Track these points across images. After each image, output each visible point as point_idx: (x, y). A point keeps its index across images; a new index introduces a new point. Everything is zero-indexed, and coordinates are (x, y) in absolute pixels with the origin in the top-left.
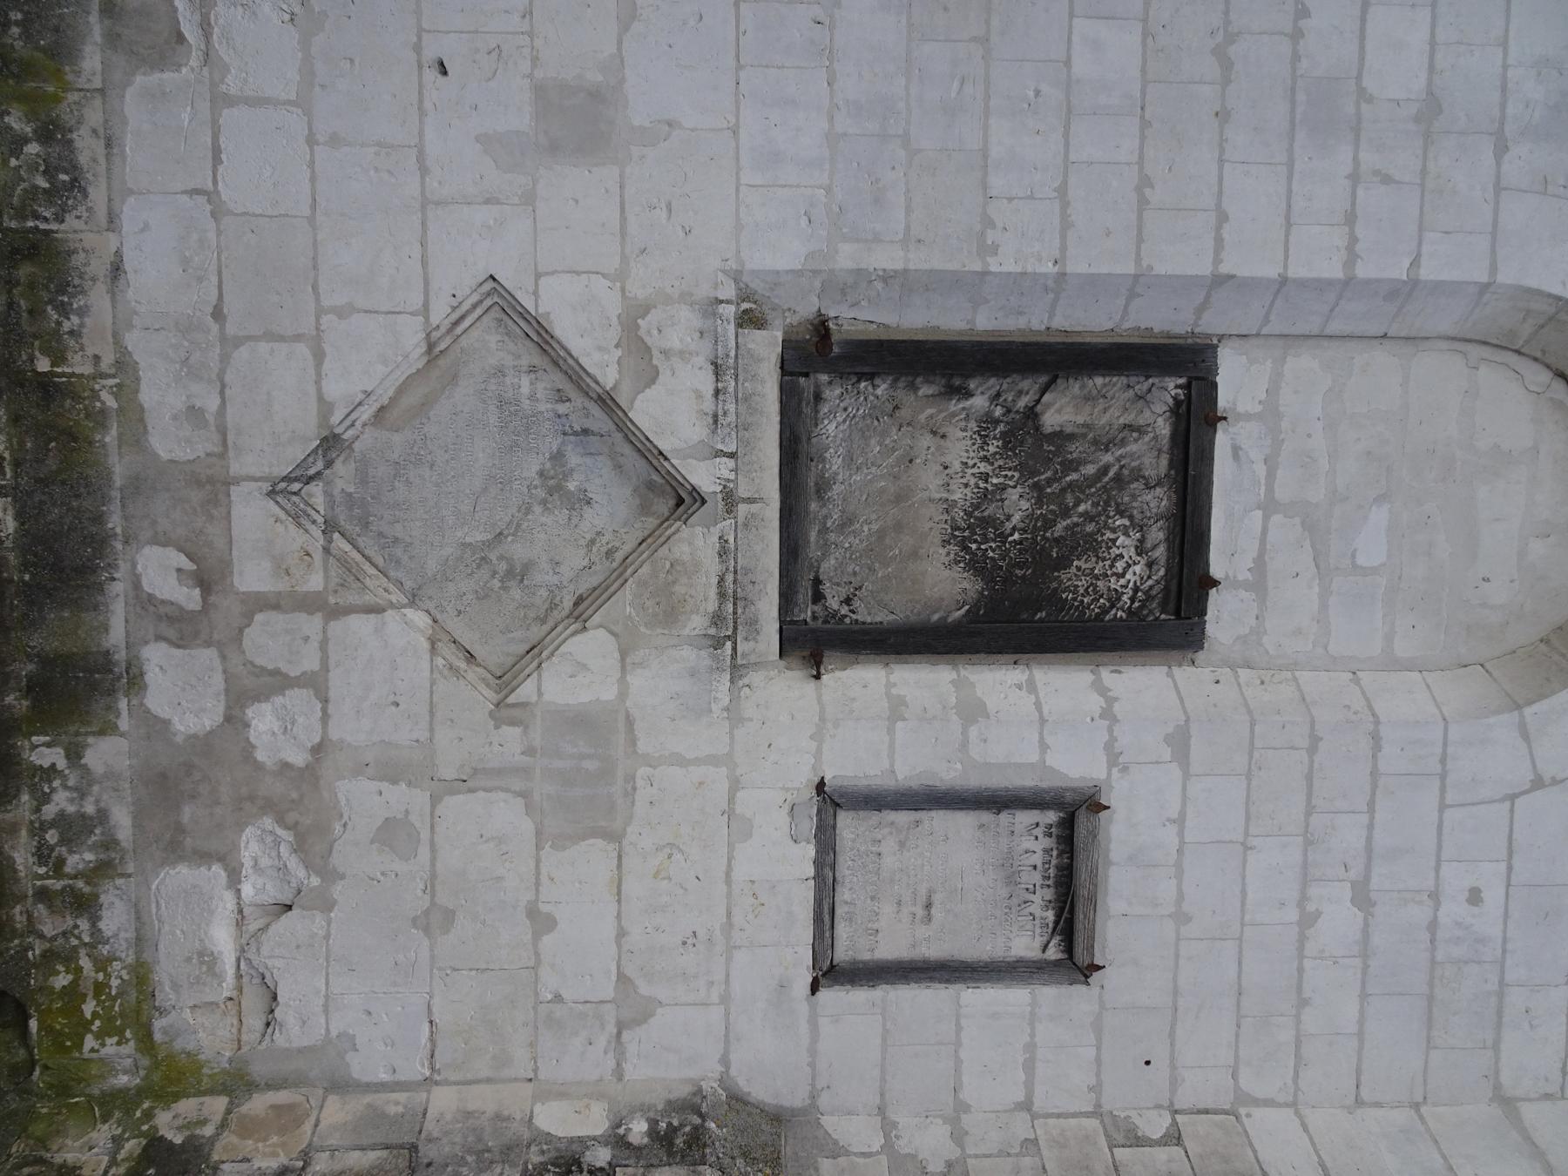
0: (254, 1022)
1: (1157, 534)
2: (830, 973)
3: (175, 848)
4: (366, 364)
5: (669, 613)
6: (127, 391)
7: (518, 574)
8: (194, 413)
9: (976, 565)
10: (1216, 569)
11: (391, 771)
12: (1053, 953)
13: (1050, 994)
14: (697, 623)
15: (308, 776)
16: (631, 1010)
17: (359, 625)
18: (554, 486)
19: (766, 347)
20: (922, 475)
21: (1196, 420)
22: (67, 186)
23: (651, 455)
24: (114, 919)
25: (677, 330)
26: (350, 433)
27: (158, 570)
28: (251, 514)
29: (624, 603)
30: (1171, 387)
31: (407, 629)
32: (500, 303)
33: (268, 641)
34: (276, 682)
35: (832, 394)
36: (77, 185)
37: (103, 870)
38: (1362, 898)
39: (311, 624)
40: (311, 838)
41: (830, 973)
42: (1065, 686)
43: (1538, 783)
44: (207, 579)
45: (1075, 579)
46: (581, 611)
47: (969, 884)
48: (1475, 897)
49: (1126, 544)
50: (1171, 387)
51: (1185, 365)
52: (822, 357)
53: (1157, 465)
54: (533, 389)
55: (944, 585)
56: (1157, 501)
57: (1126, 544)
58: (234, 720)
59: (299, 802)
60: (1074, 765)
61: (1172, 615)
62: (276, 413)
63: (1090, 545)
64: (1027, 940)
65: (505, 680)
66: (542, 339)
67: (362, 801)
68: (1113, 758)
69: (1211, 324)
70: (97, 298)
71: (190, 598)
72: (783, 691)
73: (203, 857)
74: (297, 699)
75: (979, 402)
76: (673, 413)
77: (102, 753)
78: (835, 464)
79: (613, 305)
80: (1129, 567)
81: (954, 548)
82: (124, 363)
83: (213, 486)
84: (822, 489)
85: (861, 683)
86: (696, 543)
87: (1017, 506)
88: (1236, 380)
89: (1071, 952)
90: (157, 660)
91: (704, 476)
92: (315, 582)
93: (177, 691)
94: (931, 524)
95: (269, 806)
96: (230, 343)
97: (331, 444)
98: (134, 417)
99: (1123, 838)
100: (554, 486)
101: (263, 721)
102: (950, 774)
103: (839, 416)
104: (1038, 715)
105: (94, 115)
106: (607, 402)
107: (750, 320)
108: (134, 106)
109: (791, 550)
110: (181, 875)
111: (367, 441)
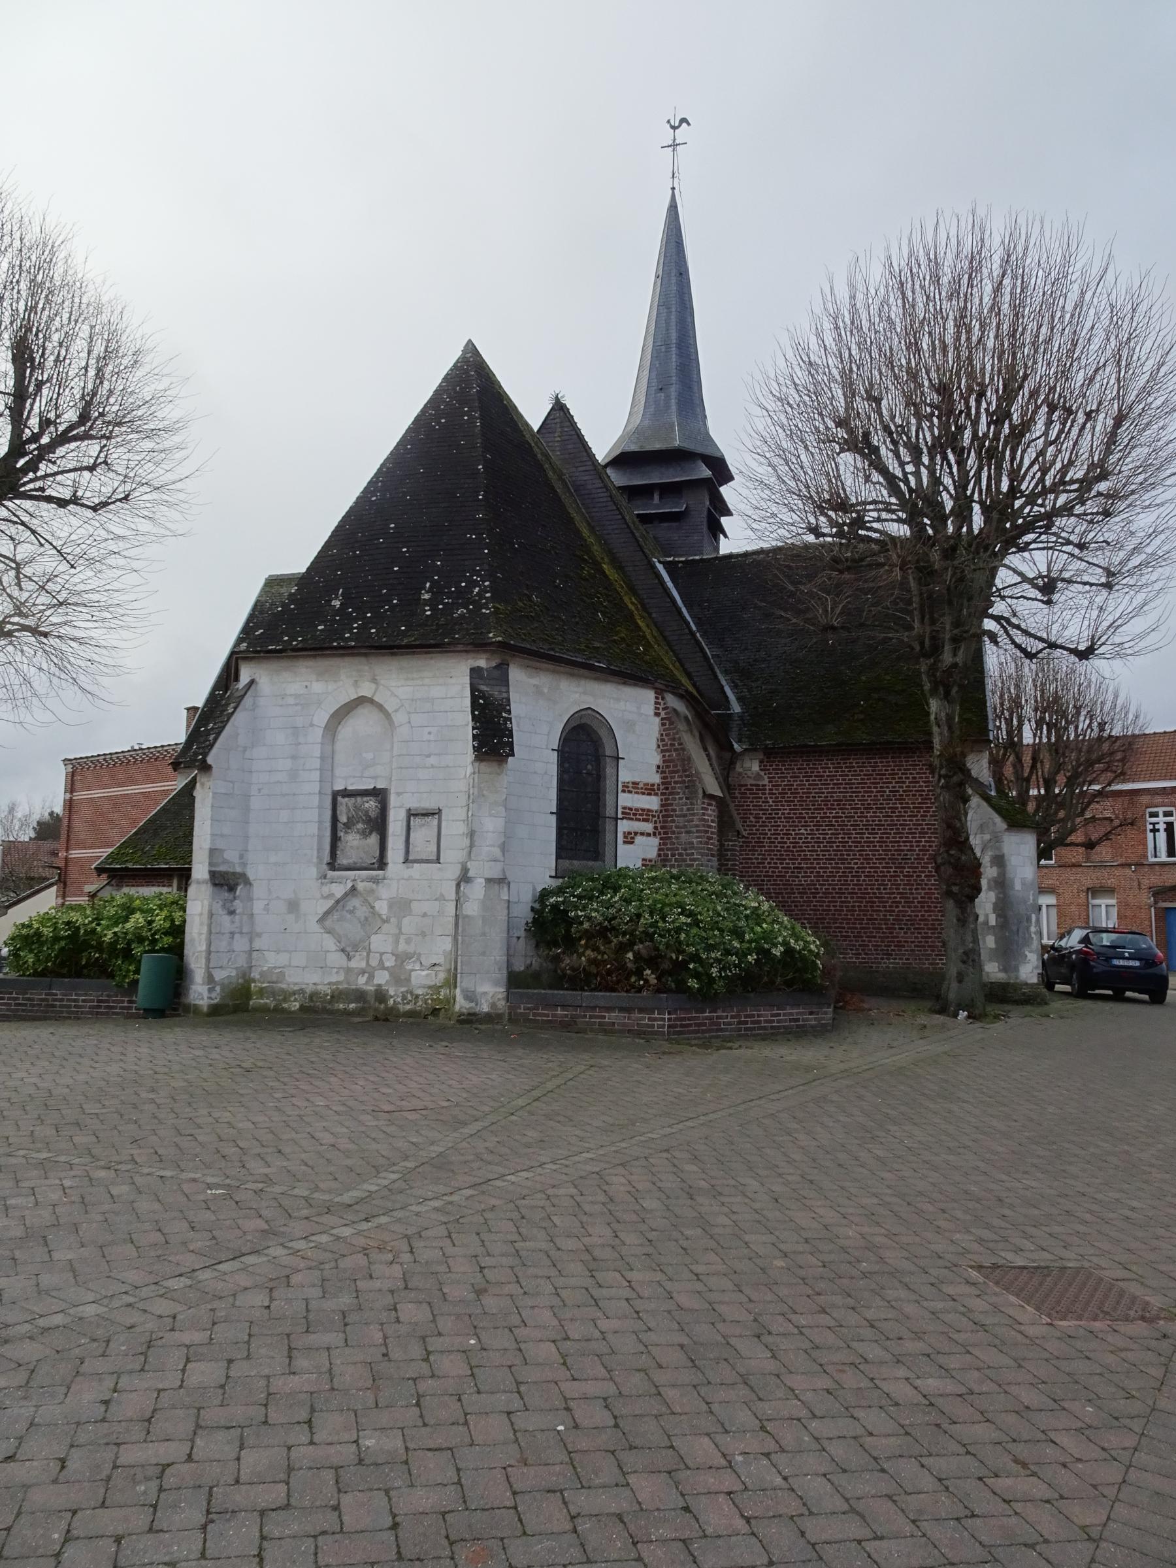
1: (365, 799)
2: (438, 861)
3: (408, 980)
4: (330, 943)
5: (372, 891)
6: (334, 984)
7: (366, 919)
9: (370, 834)
11: (397, 942)
19: (331, 874)
20: (356, 845)
21: (346, 793)
22: (302, 991)
23: (346, 895)
25: (326, 890)
28: (353, 964)
29: (370, 899)
30: (339, 798)
33: (374, 963)
38: (429, 756)
41: (438, 861)
44: (363, 972)
45: (373, 814)
46: (373, 907)
47: (423, 835)
49: (367, 805)
50: (339, 798)
51: (335, 795)
52: (332, 866)
56: (359, 799)
57: (367, 805)
58: (387, 969)
60: (402, 814)
61: (380, 795)
66: (327, 913)
67: (402, 947)
69: (329, 792)
70: (319, 987)
71: (366, 975)
76: (339, 890)
78: (351, 861)
80: (371, 804)
82: (329, 984)
83: (348, 970)
86: (361, 886)
87: (360, 826)
88: (339, 787)
89: (437, 813)
90: (376, 982)
91: (349, 885)
93: (382, 978)
97: (343, 950)
98: (338, 983)
99: (415, 803)
100: (352, 912)
101: (387, 964)
102: (403, 838)
103: (343, 861)
106: (338, 902)
110: (413, 979)
111: (343, 945)
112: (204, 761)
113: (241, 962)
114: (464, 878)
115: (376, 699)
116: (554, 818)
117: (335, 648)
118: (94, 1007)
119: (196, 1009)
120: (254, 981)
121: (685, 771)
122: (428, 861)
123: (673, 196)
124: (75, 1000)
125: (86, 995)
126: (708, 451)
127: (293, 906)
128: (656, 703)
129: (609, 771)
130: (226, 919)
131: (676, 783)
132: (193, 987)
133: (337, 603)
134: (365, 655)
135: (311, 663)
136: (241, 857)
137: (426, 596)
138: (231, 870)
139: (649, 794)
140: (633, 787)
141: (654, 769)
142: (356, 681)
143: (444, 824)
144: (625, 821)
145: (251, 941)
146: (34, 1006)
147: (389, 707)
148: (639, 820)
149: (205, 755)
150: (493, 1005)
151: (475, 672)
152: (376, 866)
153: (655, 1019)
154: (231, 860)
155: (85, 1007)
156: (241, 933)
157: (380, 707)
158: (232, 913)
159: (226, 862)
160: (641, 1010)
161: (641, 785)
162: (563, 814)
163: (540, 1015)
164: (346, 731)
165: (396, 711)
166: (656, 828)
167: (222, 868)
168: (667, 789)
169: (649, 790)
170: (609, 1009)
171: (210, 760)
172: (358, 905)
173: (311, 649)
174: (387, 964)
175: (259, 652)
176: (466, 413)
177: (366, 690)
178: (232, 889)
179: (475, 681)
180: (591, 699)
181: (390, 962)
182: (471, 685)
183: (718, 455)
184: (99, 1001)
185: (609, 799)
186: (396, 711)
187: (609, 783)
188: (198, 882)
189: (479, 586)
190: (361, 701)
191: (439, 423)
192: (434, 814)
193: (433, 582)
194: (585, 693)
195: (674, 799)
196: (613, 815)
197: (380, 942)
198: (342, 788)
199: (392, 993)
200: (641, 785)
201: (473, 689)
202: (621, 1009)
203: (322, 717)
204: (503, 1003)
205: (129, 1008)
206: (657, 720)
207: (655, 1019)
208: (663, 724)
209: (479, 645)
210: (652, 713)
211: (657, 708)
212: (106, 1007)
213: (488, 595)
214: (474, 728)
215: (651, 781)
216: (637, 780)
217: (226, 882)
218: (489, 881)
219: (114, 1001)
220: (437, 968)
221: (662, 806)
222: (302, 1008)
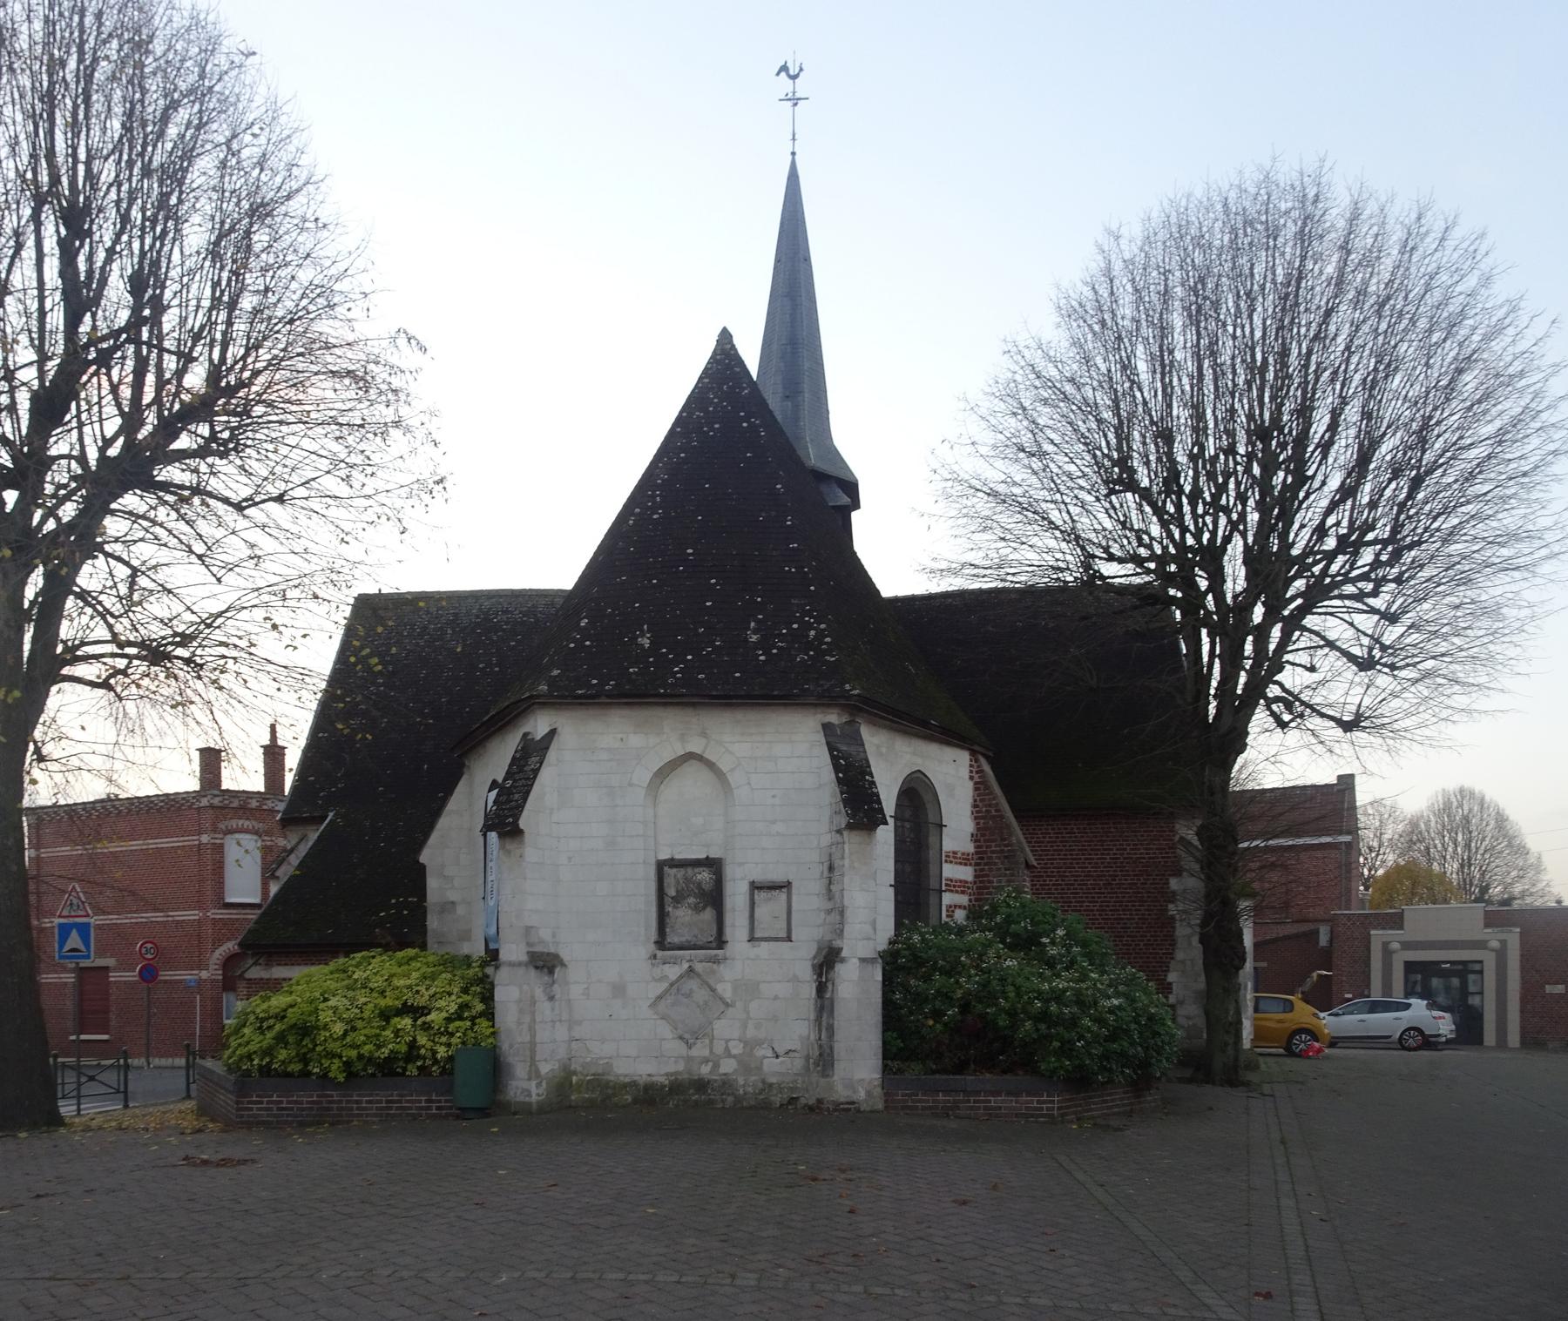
2: (789, 939)
3: (759, 1068)
4: (665, 1030)
5: (713, 972)
7: (706, 1003)
9: (704, 908)
11: (745, 1026)
13: (794, 891)
15: (746, 1043)
16: (795, 979)
18: (689, 995)
19: (660, 954)
20: (685, 920)
21: (673, 863)
22: (634, 1084)
23: (681, 977)
24: (774, 1080)
25: (658, 972)
26: (1206, 536)
27: (705, 1070)
28: (695, 1052)
29: (711, 982)
32: (653, 1005)
34: (727, 1049)
38: (774, 822)
40: (759, 1043)
41: (789, 939)
42: (729, 888)
44: (707, 1061)
46: (713, 990)
47: (770, 909)
51: (661, 866)
52: (661, 944)
53: (682, 871)
54: (670, 1000)
55: (708, 914)
56: (690, 870)
58: (734, 1057)
60: (744, 887)
61: (714, 865)
62: (675, 1048)
63: (699, 884)
65: (727, 1005)
66: (660, 997)
67: (751, 1033)
72: (729, 949)
74: (731, 1044)
76: (673, 972)
77: (741, 1081)
80: (704, 876)
83: (689, 1059)
85: (728, 933)
86: (699, 967)
87: (691, 900)
88: (664, 856)
89: (787, 886)
90: (722, 1070)
91: (686, 966)
93: (728, 1066)
97: (681, 1038)
98: (676, 1073)
99: (759, 875)
100: (689, 995)
102: (747, 914)
103: (672, 938)
106: (672, 985)
107: (655, 957)
108: (620, 1071)
110: (765, 1068)
111: (680, 1032)
114: (827, 961)
116: (892, 890)
117: (580, 697)
120: (575, 1073)
122: (776, 939)
124: (357, 1102)
126: (841, 474)
127: (619, 990)
129: (932, 840)
130: (547, 1005)
134: (694, 705)
135: (626, 712)
136: (554, 936)
137: (754, 638)
140: (954, 858)
143: (794, 898)
145: (570, 1029)
147: (724, 765)
151: (827, 727)
153: (1044, 1102)
154: (546, 939)
157: (710, 765)
158: (551, 998)
159: (542, 942)
162: (900, 885)
165: (732, 770)
167: (538, 949)
170: (997, 1093)
171: (522, 826)
172: (694, 987)
175: (566, 697)
177: (695, 746)
178: (551, 972)
180: (919, 761)
182: (828, 744)
185: (933, 869)
186: (732, 770)
187: (932, 853)
188: (512, 964)
190: (690, 756)
191: (712, 429)
193: (758, 621)
198: (667, 857)
202: (1009, 1093)
203: (644, 776)
204: (879, 1089)
205: (429, 1108)
206: (971, 784)
208: (976, 789)
209: (824, 700)
213: (828, 639)
217: (545, 963)
218: (863, 960)
222: (635, 1101)
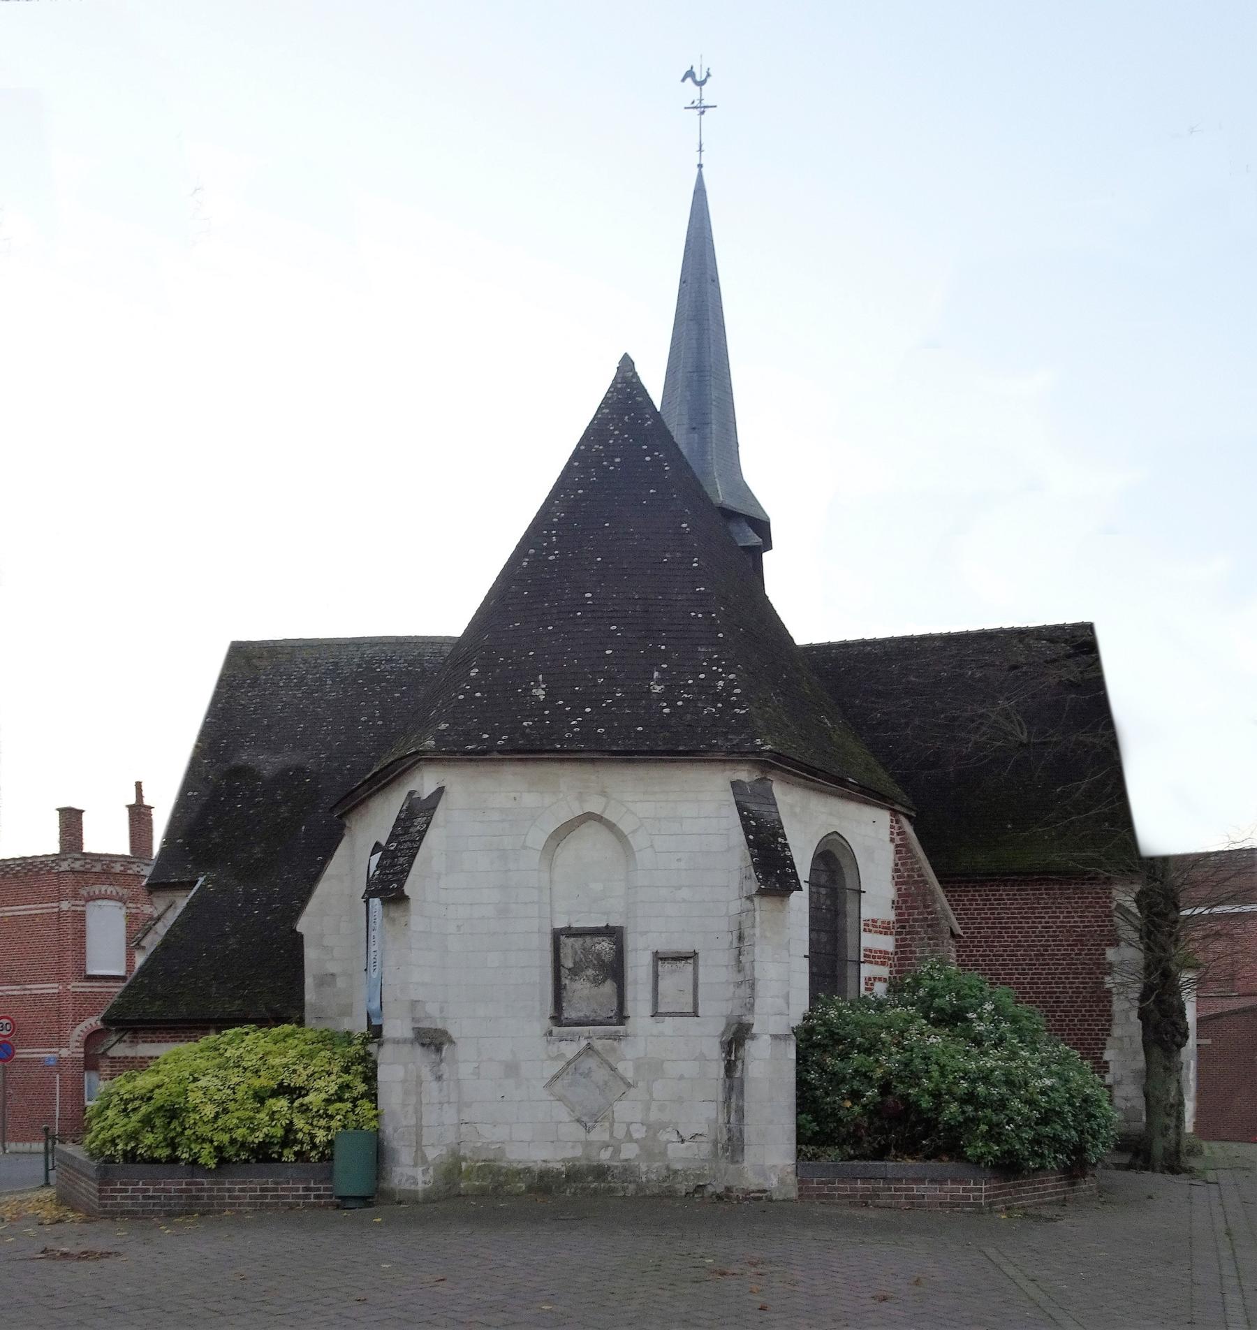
0: (703, 1139)
1: (596, 940)
3: (664, 1153)
4: (562, 1113)
5: (614, 1050)
6: (569, 1160)
7: (606, 1083)
8: (573, 1147)
9: (604, 981)
10: (604, 925)
12: (691, 961)
13: (701, 962)
14: (615, 1043)
17: (616, 1115)
18: (587, 1075)
19: (556, 1030)
20: (586, 995)
21: (570, 932)
22: (528, 1170)
23: (579, 1055)
24: (678, 1166)
25: (553, 1050)
27: (605, 1156)
29: (611, 1060)
30: (562, 938)
31: (618, 1107)
33: (620, 1132)
34: (628, 1133)
35: (566, 1015)
36: (528, 1168)
37: (668, 1168)
38: (679, 888)
39: (616, 1125)
40: (663, 1126)
43: (652, 846)
45: (607, 958)
46: (613, 1069)
47: (675, 981)
48: (679, 860)
49: (598, 947)
50: (562, 938)
51: (558, 936)
52: (557, 1019)
53: (580, 941)
55: (609, 987)
56: (588, 940)
57: (598, 947)
58: (637, 1141)
59: (653, 1128)
61: (614, 934)
64: (688, 967)
65: (629, 1086)
66: (556, 1077)
67: (654, 1116)
68: (645, 949)
69: (549, 930)
70: (550, 1165)
71: (611, 1149)
72: (631, 1026)
73: (666, 1148)
74: (633, 1127)
75: (567, 982)
76: (570, 1050)
78: (581, 1014)
79: (548, 1062)
81: (664, 1172)
82: (563, 1160)
83: (588, 1144)
84: (586, 1017)
86: (598, 1044)
87: (590, 972)
88: (561, 924)
89: (692, 957)
90: (623, 1156)
91: (584, 1043)
92: (607, 1124)
93: (629, 1152)
94: (595, 991)
95: (655, 1135)
96: (558, 1140)
97: (578, 1121)
98: (574, 1159)
99: (664, 946)
100: (587, 1075)
101: (636, 1136)
102: (650, 987)
103: (569, 1013)
104: (638, 967)
105: (515, 1165)
106: (569, 1063)
107: (551, 1033)
109: (601, 1024)
110: (669, 1153)
112: (400, 889)
113: (451, 1138)
114: (737, 1038)
115: (605, 816)
118: (256, 1197)
119: (410, 1199)
120: (464, 1159)
121: (926, 907)
122: (682, 1015)
123: (700, 176)
124: (229, 1190)
125: (244, 1183)
127: (512, 1069)
128: (892, 827)
129: (850, 907)
131: (915, 920)
132: (398, 1170)
133: (540, 693)
135: (519, 769)
136: (442, 1011)
137: (658, 689)
138: (433, 1026)
139: (886, 934)
141: (890, 904)
142: (581, 793)
143: (701, 970)
144: (866, 965)
145: (459, 1111)
146: (171, 1198)
147: (625, 827)
148: (877, 963)
149: (401, 883)
150: (782, 1181)
151: (735, 785)
152: (614, 1020)
153: (971, 1190)
154: (434, 1016)
155: (245, 1197)
156: (449, 1103)
157: (611, 826)
158: (439, 1078)
159: (428, 1017)
160: (954, 1181)
161: (879, 924)
163: (835, 1189)
164: (568, 853)
165: (634, 832)
166: (891, 972)
168: (904, 927)
169: (885, 929)
170: (920, 1180)
173: (519, 752)
174: (636, 1136)
175: (454, 753)
176: (647, 453)
178: (439, 1049)
179: (741, 798)
181: (639, 1133)
182: (737, 803)
183: (762, 517)
184: (262, 1190)
185: (851, 938)
188: (397, 1042)
189: (723, 679)
190: (589, 817)
192: (687, 958)
194: (831, 814)
195: (913, 939)
196: (855, 958)
197: (627, 1111)
199: (644, 1168)
200: (879, 924)
201: (741, 808)
202: (932, 1181)
203: (538, 837)
204: (793, 1177)
206: (891, 847)
207: (971, 1190)
208: (897, 852)
210: (888, 839)
211: (892, 833)
212: (272, 1197)
214: (752, 856)
215: (887, 919)
216: (875, 917)
217: (433, 1040)
218: (775, 1037)
219: (283, 1190)
220: (698, 1139)
221: (897, 947)
